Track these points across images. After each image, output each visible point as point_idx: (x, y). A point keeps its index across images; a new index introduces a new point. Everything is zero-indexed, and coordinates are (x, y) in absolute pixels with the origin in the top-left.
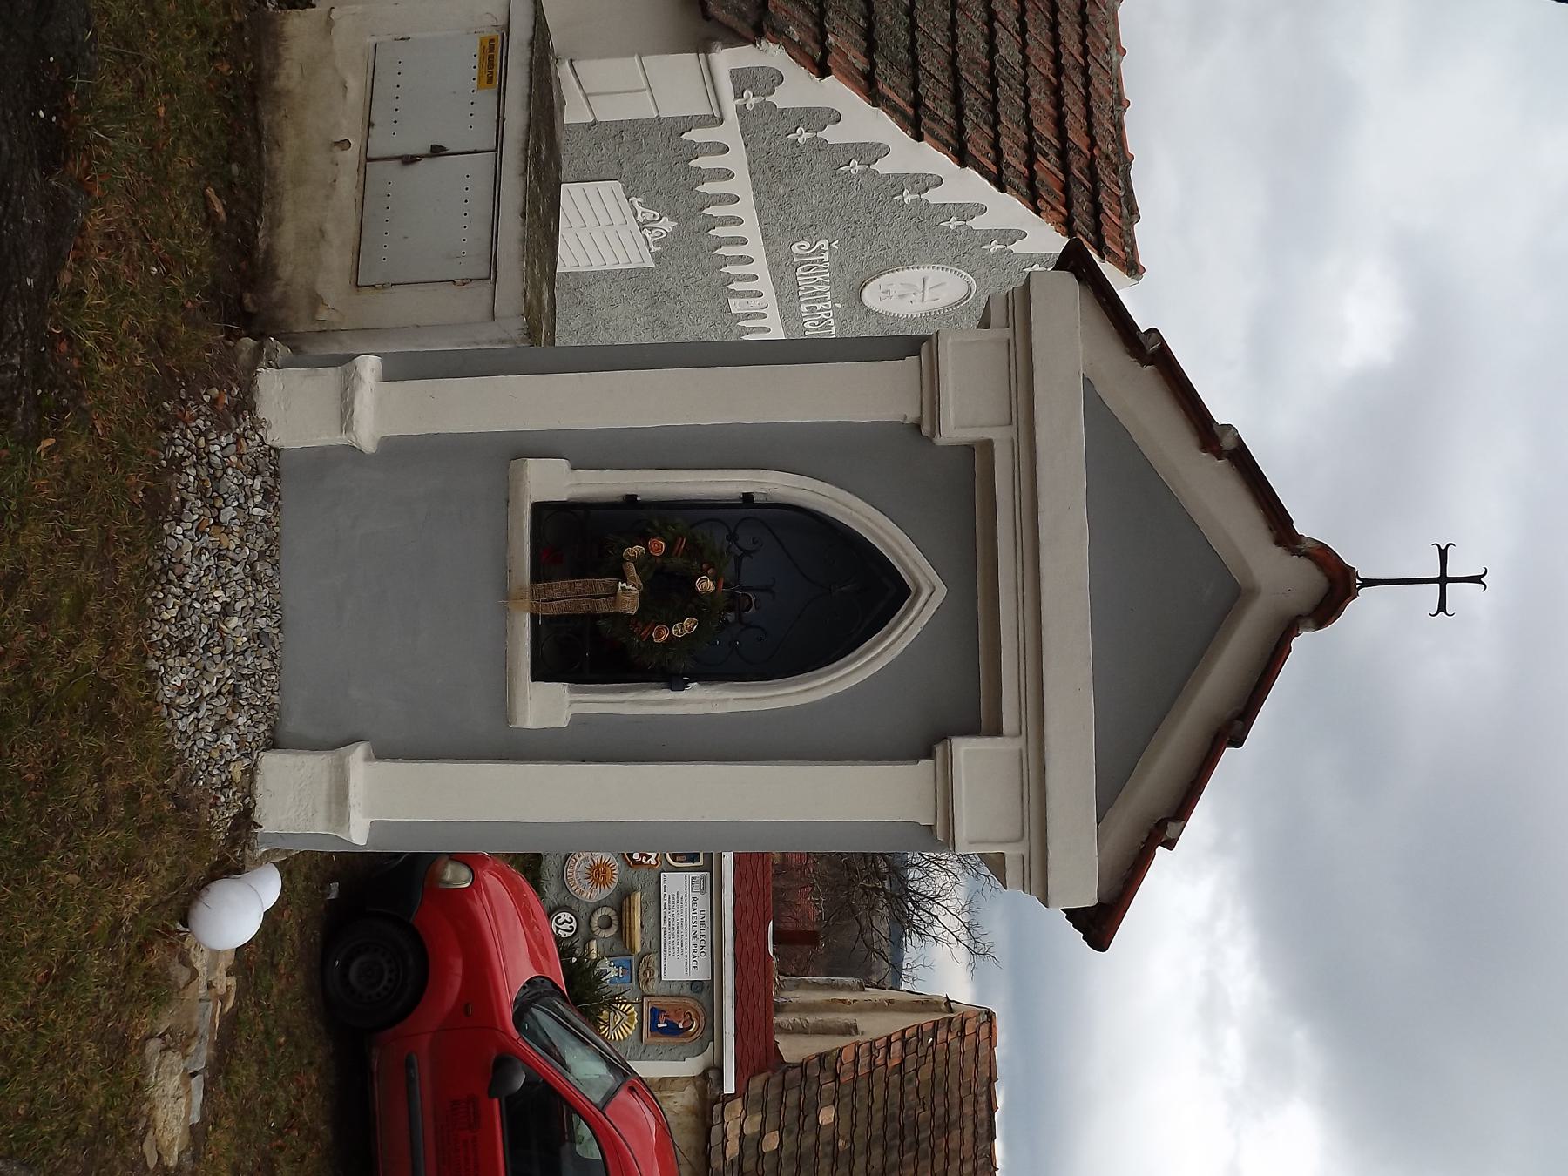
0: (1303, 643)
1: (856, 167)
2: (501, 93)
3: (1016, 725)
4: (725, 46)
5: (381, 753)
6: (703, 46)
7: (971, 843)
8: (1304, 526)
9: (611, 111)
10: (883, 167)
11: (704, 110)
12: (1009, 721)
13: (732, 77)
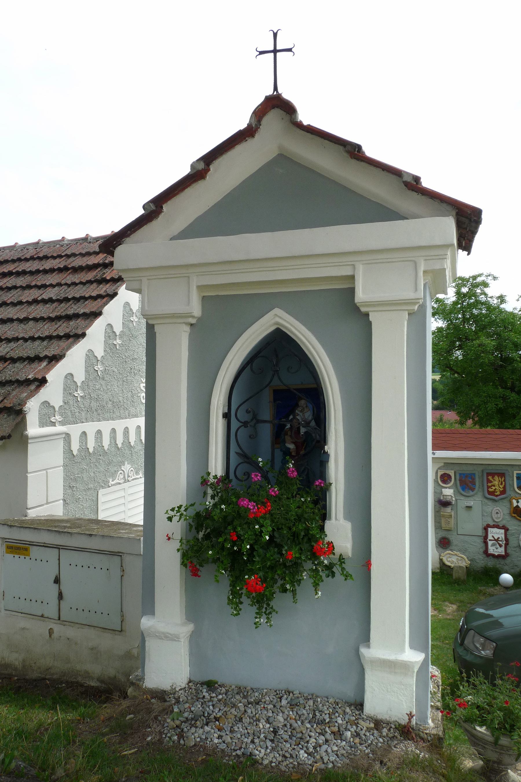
0: (305, 117)
1: (99, 367)
2: (32, 544)
3: (349, 267)
4: (26, 429)
5: (366, 639)
6: (24, 441)
7: (416, 290)
8: (242, 124)
9: (57, 490)
10: (99, 353)
11: (60, 444)
12: (346, 271)
13: (43, 427)
